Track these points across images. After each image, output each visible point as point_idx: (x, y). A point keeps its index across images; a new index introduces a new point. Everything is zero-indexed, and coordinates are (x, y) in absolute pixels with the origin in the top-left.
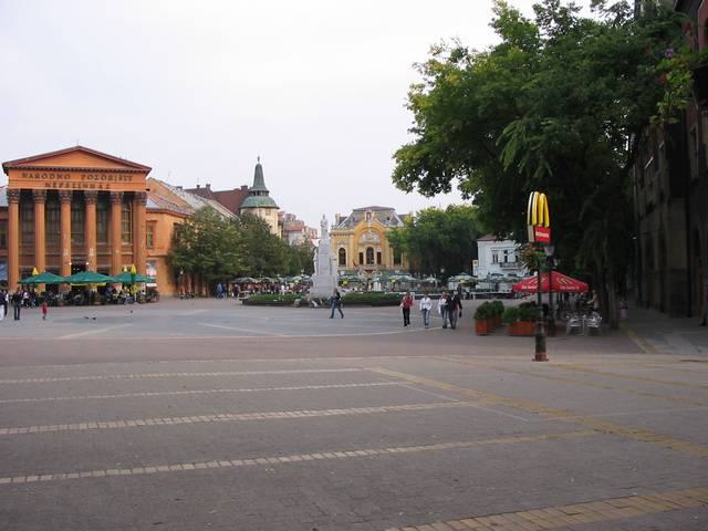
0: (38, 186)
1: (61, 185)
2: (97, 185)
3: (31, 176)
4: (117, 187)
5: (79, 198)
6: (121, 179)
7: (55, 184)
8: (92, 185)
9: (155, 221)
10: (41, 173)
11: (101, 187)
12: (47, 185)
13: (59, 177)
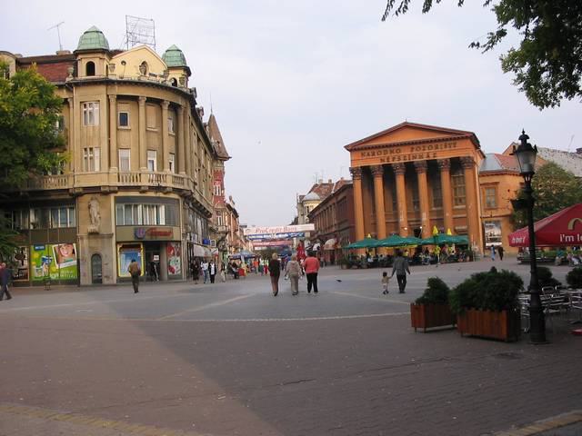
0: (374, 162)
1: (394, 159)
2: (425, 155)
3: (368, 155)
4: (443, 154)
5: (411, 170)
6: (446, 147)
7: (388, 159)
8: (405, 155)
9: (497, 183)
10: (376, 151)
11: (428, 156)
12: (382, 160)
13: (392, 152)
